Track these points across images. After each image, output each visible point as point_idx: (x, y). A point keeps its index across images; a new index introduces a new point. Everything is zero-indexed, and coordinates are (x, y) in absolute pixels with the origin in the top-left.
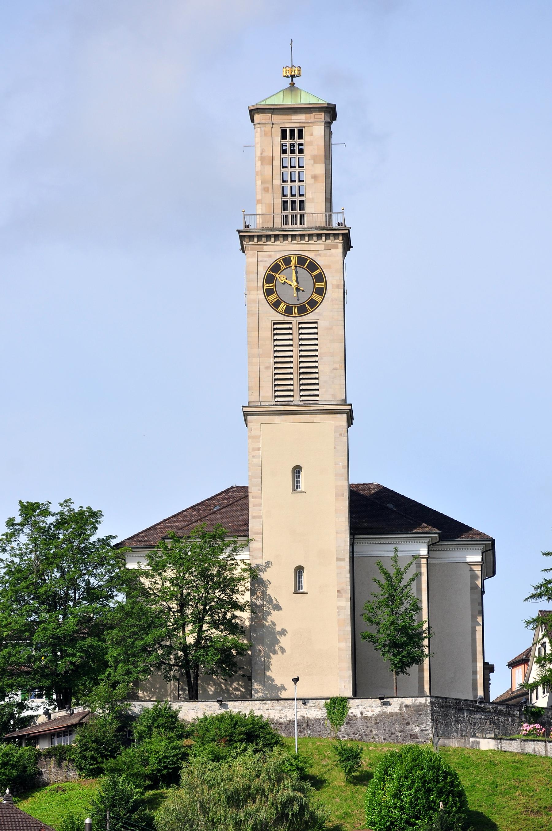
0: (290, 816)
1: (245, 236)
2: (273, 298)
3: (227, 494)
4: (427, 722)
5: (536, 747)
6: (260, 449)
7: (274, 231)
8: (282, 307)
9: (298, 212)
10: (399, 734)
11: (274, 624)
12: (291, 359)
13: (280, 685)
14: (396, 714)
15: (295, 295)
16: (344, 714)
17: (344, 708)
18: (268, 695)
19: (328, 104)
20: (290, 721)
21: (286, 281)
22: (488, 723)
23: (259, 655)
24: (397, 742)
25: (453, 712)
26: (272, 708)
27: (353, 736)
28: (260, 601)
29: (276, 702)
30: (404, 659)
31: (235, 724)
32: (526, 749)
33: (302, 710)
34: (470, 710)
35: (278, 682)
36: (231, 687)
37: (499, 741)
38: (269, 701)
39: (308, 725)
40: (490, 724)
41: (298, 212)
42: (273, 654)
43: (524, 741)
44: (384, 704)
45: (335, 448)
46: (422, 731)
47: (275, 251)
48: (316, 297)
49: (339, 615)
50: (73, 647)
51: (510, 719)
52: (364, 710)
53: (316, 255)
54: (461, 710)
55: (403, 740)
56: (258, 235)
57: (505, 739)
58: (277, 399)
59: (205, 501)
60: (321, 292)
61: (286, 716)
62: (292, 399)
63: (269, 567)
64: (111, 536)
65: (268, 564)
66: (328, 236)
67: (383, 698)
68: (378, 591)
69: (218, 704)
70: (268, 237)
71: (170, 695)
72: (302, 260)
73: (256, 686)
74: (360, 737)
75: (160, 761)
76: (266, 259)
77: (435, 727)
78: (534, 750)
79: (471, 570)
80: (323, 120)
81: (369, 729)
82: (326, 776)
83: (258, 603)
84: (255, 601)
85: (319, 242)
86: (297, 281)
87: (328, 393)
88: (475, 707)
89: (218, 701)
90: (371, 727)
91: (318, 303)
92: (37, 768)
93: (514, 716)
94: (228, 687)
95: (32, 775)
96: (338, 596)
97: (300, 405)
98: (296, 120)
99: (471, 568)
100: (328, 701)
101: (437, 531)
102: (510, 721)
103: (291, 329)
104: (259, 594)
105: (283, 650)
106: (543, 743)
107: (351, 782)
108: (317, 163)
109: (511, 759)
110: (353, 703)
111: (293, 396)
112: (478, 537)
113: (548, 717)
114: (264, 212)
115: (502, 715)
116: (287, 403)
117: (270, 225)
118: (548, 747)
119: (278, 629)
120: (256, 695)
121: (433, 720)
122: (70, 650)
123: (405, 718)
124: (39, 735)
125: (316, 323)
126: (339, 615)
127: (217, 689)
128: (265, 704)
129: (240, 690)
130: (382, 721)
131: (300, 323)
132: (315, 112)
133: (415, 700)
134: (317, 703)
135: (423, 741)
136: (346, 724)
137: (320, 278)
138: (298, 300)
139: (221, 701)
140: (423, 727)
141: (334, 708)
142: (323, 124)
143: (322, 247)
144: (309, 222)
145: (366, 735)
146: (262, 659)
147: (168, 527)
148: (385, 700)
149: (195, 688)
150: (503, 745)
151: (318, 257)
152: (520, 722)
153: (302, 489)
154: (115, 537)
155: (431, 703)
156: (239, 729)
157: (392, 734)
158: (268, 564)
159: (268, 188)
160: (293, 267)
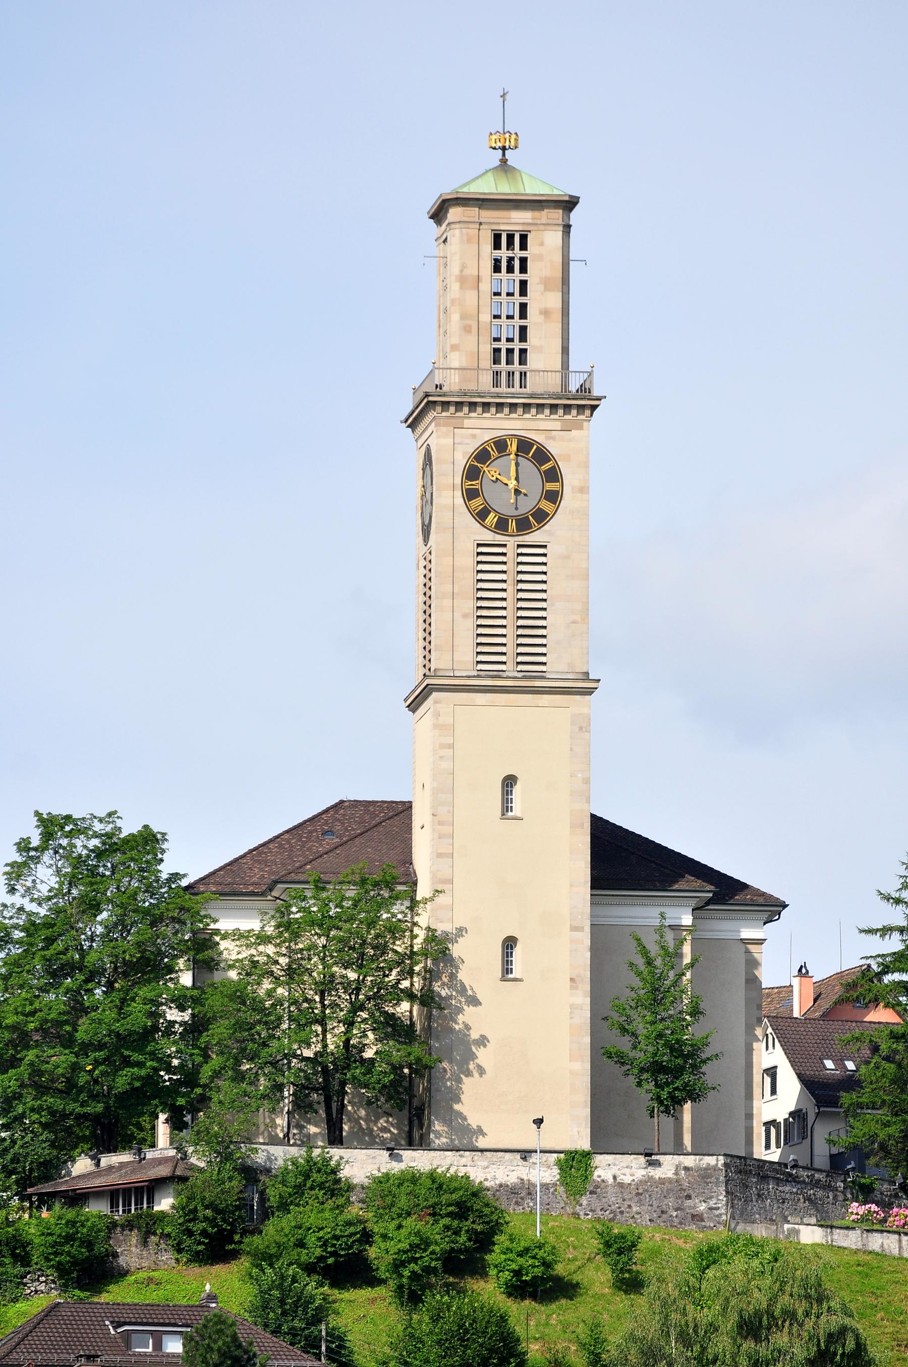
0: (838, 1357)
1: (435, 402)
2: (477, 503)
3: (337, 812)
4: (718, 1195)
5: (886, 1242)
6: (451, 746)
7: (482, 397)
8: (491, 519)
9: (516, 366)
10: (675, 1214)
11: (468, 1027)
12: (503, 604)
13: (475, 1127)
14: (670, 1180)
15: (512, 501)
16: (586, 1178)
17: (588, 1166)
18: (456, 1142)
19: (570, 196)
20: (501, 1185)
21: (499, 477)
22: (802, 1200)
23: (444, 1077)
24: (671, 1226)
25: (755, 1180)
26: (472, 1164)
27: (600, 1213)
28: (447, 990)
29: (479, 1153)
30: (677, 1093)
31: (440, 1187)
32: (870, 1244)
33: (521, 1168)
34: (778, 1179)
35: (473, 1121)
36: (375, 1124)
37: (829, 1230)
38: (468, 1153)
39: (530, 1194)
40: (804, 1202)
41: (516, 366)
42: (466, 1076)
43: (868, 1231)
44: (650, 1164)
45: (571, 749)
46: (711, 1209)
47: (482, 428)
48: (546, 506)
49: (571, 1018)
50: (141, 1051)
51: (831, 1195)
52: (618, 1173)
53: (547, 438)
54: (764, 1178)
55: (681, 1223)
56: (578, 406)
57: (838, 1228)
58: (480, 667)
59: (305, 822)
60: (554, 497)
61: (495, 1178)
62: (503, 667)
63: (462, 936)
64: (177, 874)
65: (461, 931)
66: (567, 408)
67: (650, 1155)
68: (637, 982)
69: (386, 1154)
70: (473, 406)
71: (263, 1133)
72: (524, 446)
73: (437, 1126)
74: (612, 1215)
75: (325, 1244)
76: (467, 441)
77: (731, 1204)
78: (882, 1246)
79: (748, 952)
80: (560, 222)
81: (627, 1203)
82: (576, 1278)
83: (443, 994)
84: (439, 989)
85: (498, 415)
86: (517, 479)
87: (558, 664)
88: (784, 1173)
89: (388, 1149)
90: (630, 1199)
91: (549, 514)
92: (110, 1245)
93: (837, 1190)
94: (371, 1125)
95: (103, 1257)
96: (572, 988)
97: (516, 678)
98: (517, 219)
99: (747, 949)
100: (562, 1156)
101: (712, 888)
102: (831, 1197)
103: (504, 554)
104: (445, 980)
105: (481, 1071)
106: (896, 1236)
107: (620, 1289)
108: (549, 290)
109: (853, 1259)
110: (600, 1160)
111: (505, 663)
112: (761, 900)
113: (882, 1194)
114: (464, 365)
115: (820, 1188)
116: (495, 673)
117: (472, 387)
118: (904, 1243)
119: (474, 1035)
120: (437, 1141)
121: (727, 1192)
122: (136, 1057)
123: (684, 1187)
124: (88, 1193)
125: (545, 547)
126: (571, 1018)
127: (353, 1128)
128: (461, 1156)
129: (390, 1131)
130: (647, 1191)
131: (519, 546)
132: (548, 207)
133: (700, 1160)
134: (544, 1159)
135: (712, 1225)
136: (590, 1193)
137: (553, 475)
138: (517, 509)
139: (393, 1149)
140: (712, 1203)
141: (572, 1167)
142: (561, 228)
143: (557, 425)
144: (534, 384)
145: (622, 1213)
146: (449, 1084)
147: (259, 862)
148: (654, 1157)
149: (338, 1125)
150: (835, 1237)
151: (551, 441)
152: (846, 1200)
153: (517, 811)
154: (185, 876)
155: (726, 1165)
156: (444, 1198)
157: (663, 1212)
158: (461, 931)
159: (470, 327)
160: (512, 456)
